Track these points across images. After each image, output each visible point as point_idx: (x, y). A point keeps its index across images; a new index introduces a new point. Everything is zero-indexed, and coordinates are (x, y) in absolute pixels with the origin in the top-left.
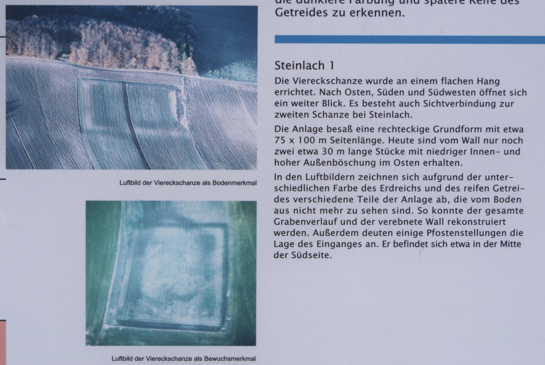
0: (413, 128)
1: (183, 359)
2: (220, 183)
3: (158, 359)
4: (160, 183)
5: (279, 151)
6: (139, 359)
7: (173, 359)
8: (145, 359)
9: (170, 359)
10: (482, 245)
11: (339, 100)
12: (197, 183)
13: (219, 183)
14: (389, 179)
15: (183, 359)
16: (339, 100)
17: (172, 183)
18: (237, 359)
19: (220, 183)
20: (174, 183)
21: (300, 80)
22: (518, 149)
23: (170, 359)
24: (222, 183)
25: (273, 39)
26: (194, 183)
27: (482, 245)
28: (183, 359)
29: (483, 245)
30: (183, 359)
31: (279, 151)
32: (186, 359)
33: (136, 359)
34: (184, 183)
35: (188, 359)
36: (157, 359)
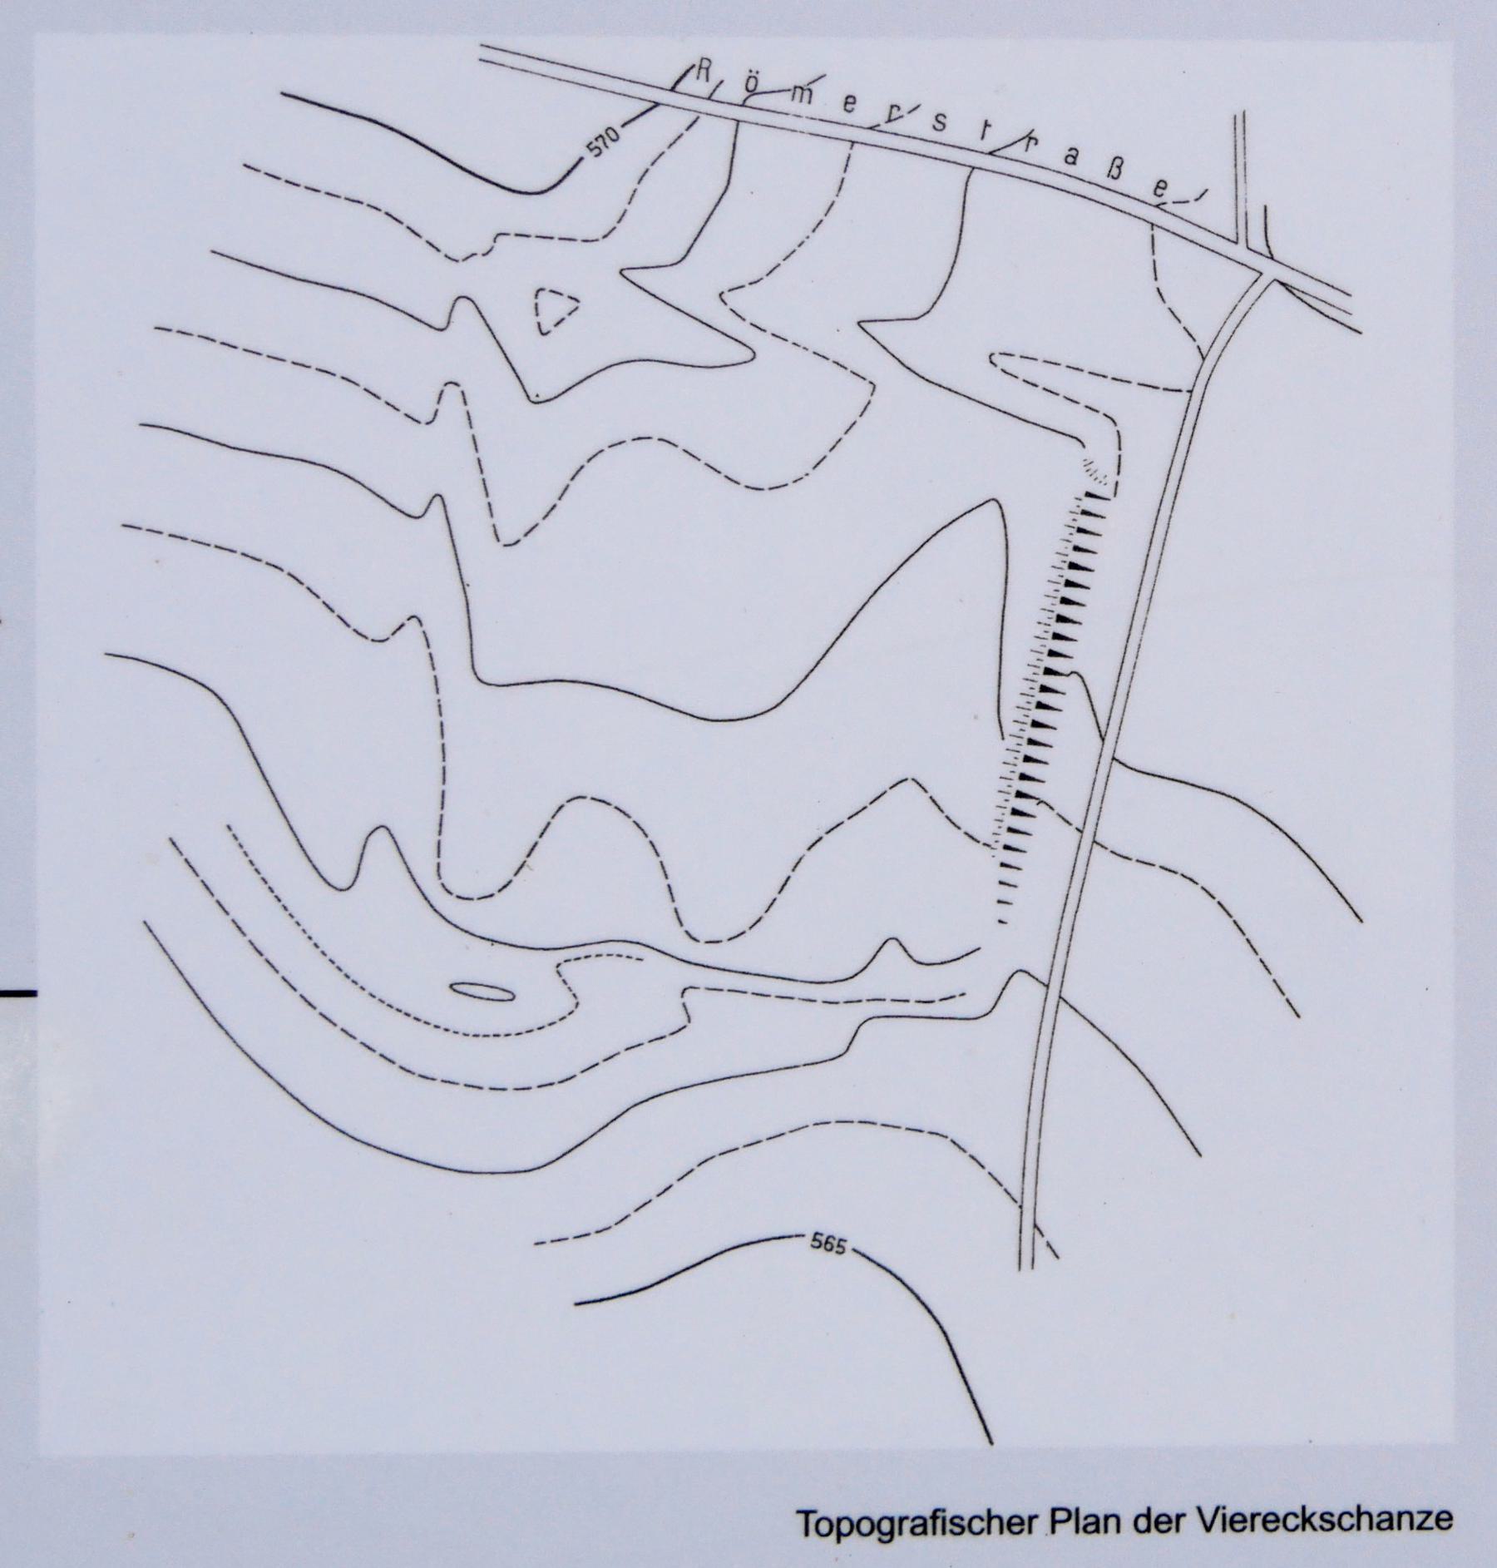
0: (1307, 1515)
1: (1405, 1519)
2: (855, 1526)
3: (1265, 1522)
4: (1232, 1522)
5: (1417, 1522)
6: (1157, 1523)
7: (977, 1525)
8: (1191, 1523)
9: (1330, 1522)
10: (1127, 1524)
11: (1304, 1508)
12: (1438, 1520)
13: (865, 1526)
14: (1157, 1527)
15: (1405, 1519)
16: (1304, 1508)
17: (1299, 1521)
18: (1010, 1524)
19: (855, 1526)
20: (1306, 1520)
21: (1224, 1516)
22: (843, 1539)
23: (1330, 1522)
24: (845, 1527)
25: (39, 994)
26: (1418, 1519)
27: (1127, 1524)
28: (1405, 1519)
29: (1132, 1527)
30: (1405, 1519)
31: (1417, 1522)
32: (1418, 1519)
33: (1142, 1523)
34: (1365, 1519)
35: (1431, 1522)
36: (1258, 1521)
